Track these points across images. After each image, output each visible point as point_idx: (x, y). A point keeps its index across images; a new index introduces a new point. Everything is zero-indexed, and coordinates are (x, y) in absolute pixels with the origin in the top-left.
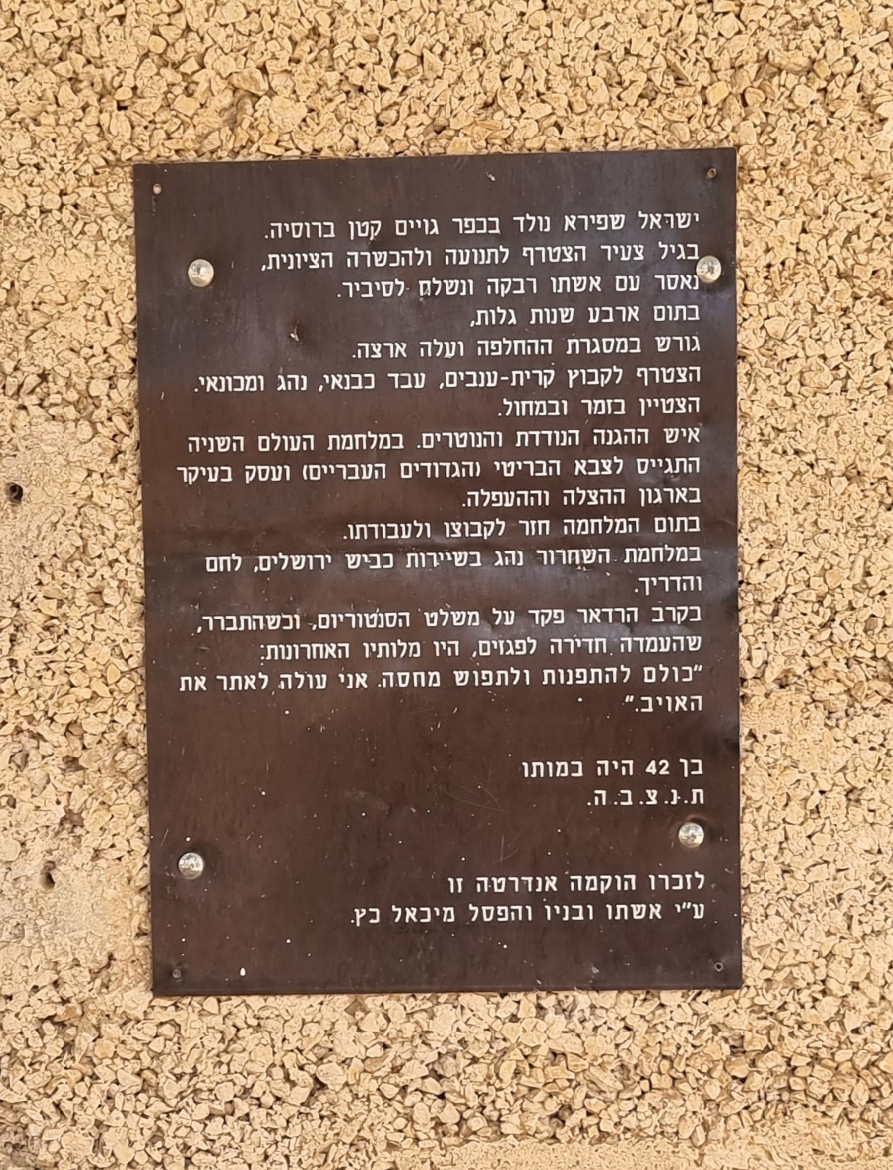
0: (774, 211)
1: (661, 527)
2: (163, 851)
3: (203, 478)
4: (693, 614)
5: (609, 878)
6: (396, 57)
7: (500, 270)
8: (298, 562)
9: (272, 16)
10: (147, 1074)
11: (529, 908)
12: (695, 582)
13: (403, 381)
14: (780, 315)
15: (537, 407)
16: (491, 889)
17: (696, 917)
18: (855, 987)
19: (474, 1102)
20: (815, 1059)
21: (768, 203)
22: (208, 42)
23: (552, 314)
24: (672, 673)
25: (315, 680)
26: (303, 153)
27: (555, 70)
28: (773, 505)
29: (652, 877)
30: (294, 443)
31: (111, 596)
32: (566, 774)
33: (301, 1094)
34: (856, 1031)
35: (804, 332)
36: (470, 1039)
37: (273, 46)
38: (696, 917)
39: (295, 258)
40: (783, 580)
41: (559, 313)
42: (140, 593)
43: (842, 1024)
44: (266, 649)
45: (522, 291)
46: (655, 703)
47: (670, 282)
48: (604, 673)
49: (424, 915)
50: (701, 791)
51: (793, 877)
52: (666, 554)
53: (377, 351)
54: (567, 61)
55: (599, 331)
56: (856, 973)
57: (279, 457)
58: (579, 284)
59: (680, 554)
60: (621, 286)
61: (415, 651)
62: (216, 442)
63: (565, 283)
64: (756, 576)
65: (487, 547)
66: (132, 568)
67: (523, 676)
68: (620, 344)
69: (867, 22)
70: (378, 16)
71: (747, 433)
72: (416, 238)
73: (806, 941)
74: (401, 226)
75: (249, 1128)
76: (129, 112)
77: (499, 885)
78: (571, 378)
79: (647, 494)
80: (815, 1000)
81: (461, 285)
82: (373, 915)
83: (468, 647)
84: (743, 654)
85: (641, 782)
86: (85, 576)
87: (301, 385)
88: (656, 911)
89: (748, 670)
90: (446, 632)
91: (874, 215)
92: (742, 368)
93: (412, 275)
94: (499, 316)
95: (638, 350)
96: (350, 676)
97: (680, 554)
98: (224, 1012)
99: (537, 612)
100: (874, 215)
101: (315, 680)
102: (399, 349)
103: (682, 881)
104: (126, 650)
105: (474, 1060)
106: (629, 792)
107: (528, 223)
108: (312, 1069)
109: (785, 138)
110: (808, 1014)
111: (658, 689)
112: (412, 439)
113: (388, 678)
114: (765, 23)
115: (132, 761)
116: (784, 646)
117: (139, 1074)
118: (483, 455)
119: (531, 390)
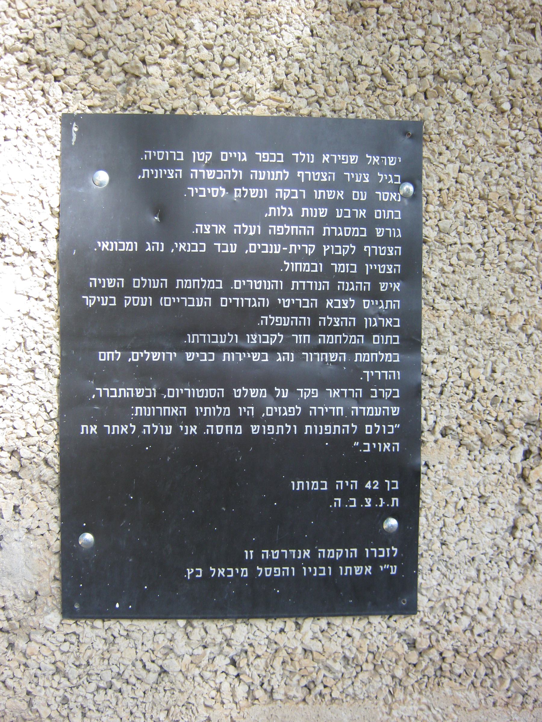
0: (444, 159)
1: (376, 341)
2: (69, 530)
3: (98, 304)
4: (394, 393)
5: (342, 550)
6: (224, 58)
7: (283, 184)
8: (156, 356)
9: (150, 31)
10: (59, 664)
11: (293, 568)
12: (396, 374)
13: (223, 248)
14: (446, 218)
15: (304, 267)
16: (270, 557)
17: (392, 573)
18: (480, 610)
19: (257, 681)
20: (457, 651)
21: (440, 154)
22: (111, 44)
23: (314, 211)
24: (382, 428)
25: (165, 429)
26: (166, 111)
27: (318, 70)
28: (442, 329)
29: (367, 550)
30: (155, 284)
31: (40, 373)
32: (317, 489)
33: (153, 677)
34: (479, 635)
35: (461, 229)
36: (255, 644)
37: (150, 48)
38: (392, 573)
39: (159, 172)
40: (446, 374)
41: (318, 211)
42: (58, 372)
43: (472, 631)
44: (135, 409)
45: (296, 197)
46: (372, 446)
47: (384, 196)
48: (342, 428)
49: (229, 572)
50: (397, 499)
51: (448, 548)
52: (380, 357)
53: (208, 230)
54: (325, 66)
55: (343, 223)
56: (481, 603)
57: (144, 292)
58: (330, 195)
59: (388, 357)
60: (356, 197)
61: (227, 413)
62: (106, 281)
63: (322, 193)
64: (430, 370)
65: (273, 350)
66: (53, 356)
67: (293, 429)
68: (354, 231)
69: (496, 57)
70: (214, 34)
71: (428, 286)
72: (233, 163)
73: (454, 585)
74: (224, 155)
75: (121, 697)
76: (62, 83)
77: (275, 555)
78: (325, 250)
79: (368, 321)
80: (457, 618)
81: (259, 192)
82: (198, 573)
83: (260, 410)
84: (423, 416)
85: (362, 493)
86: (24, 361)
87: (160, 248)
88: (368, 570)
89: (425, 425)
90: (246, 401)
91: (500, 165)
92: (425, 247)
93: (230, 185)
94: (282, 211)
95: (365, 235)
96: (187, 427)
97: (388, 357)
98: (106, 627)
99: (302, 390)
100: (500, 165)
101: (165, 429)
102: (221, 229)
103: (384, 552)
104: (49, 407)
105: (258, 656)
106: (354, 499)
107: (301, 157)
108: (160, 662)
109: (450, 118)
110: (454, 626)
111: (373, 438)
112: (228, 283)
113: (210, 428)
114: (438, 53)
115: (51, 475)
116: (445, 413)
117: (54, 663)
118: (272, 295)
119: (301, 256)
